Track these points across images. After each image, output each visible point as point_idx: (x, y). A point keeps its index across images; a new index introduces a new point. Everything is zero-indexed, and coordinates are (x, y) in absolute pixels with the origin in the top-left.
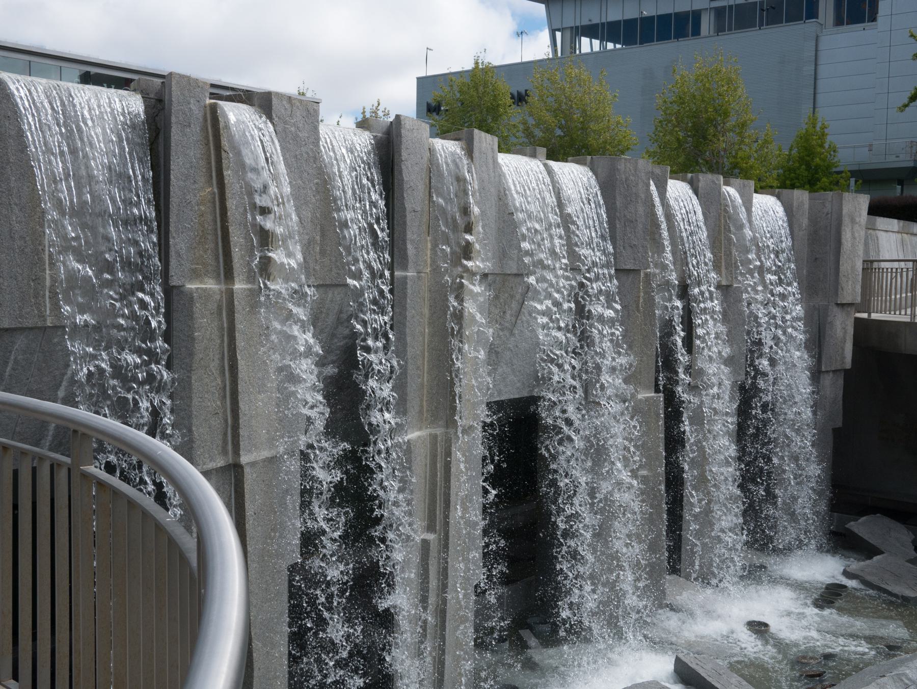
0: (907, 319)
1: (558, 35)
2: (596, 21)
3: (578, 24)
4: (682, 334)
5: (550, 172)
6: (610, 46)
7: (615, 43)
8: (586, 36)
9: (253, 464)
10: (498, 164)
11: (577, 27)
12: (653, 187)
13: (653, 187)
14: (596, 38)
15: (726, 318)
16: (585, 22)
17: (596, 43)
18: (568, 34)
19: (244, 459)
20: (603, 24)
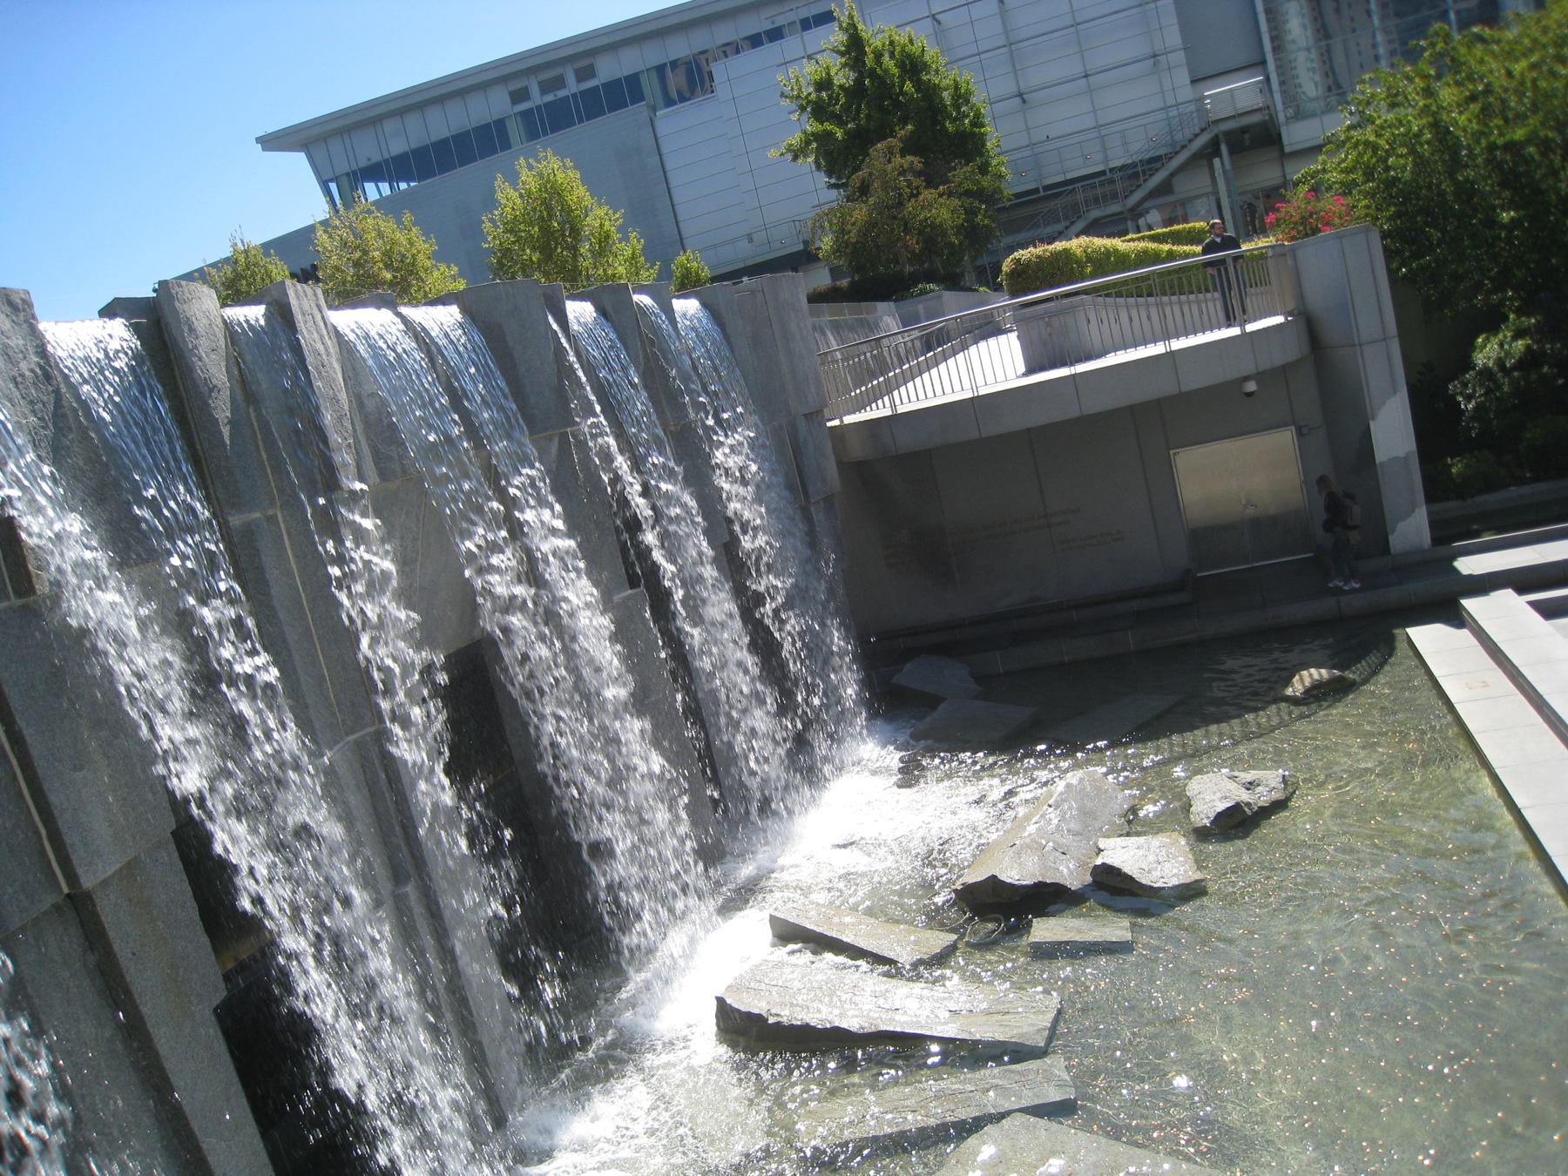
0: (888, 412)
1: (333, 186)
2: (376, 158)
3: (354, 167)
4: (734, 506)
5: (399, 315)
6: (403, 186)
7: (408, 180)
8: (369, 181)
9: (105, 883)
10: (340, 819)
11: (354, 173)
12: (551, 319)
13: (551, 319)
14: (383, 180)
15: (563, 490)
16: (363, 163)
17: (385, 188)
18: (345, 181)
19: (88, 882)
20: (386, 161)
